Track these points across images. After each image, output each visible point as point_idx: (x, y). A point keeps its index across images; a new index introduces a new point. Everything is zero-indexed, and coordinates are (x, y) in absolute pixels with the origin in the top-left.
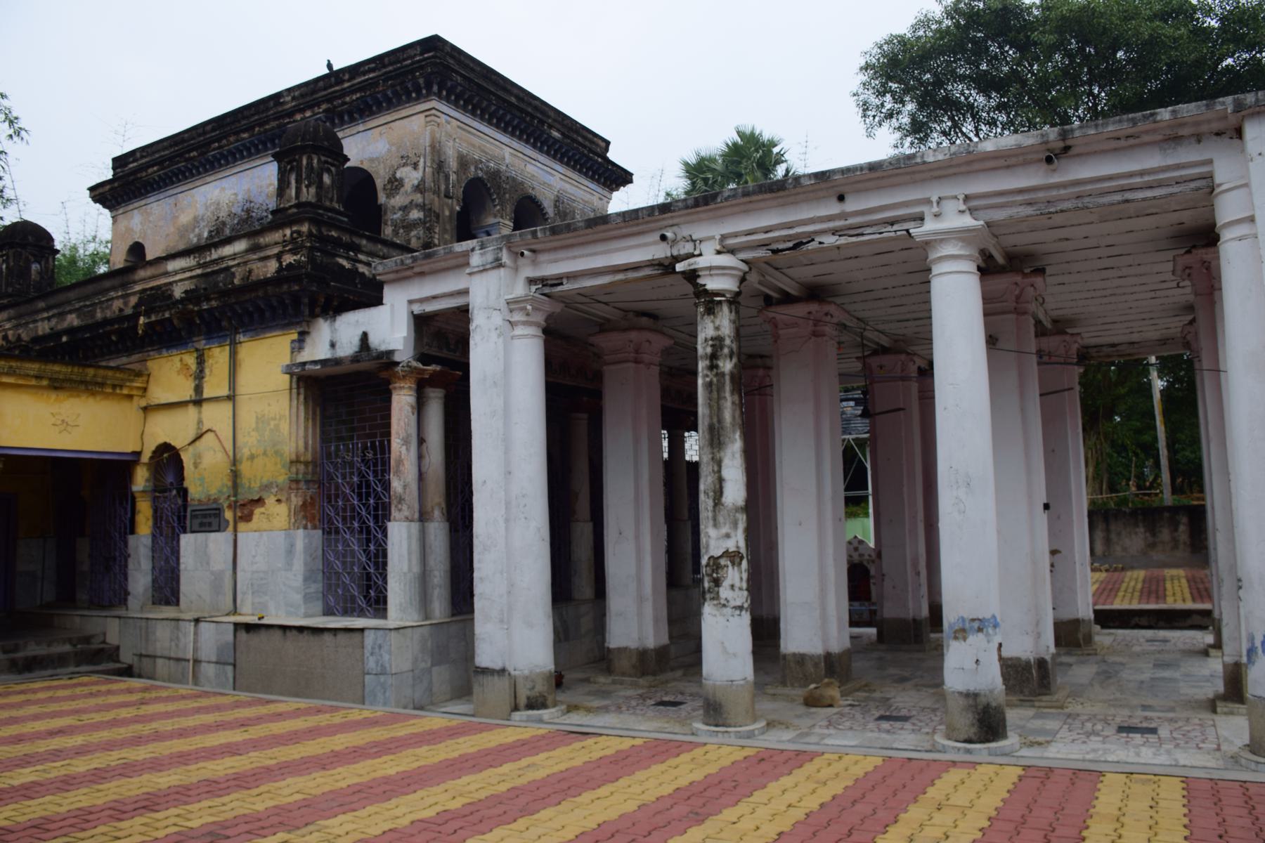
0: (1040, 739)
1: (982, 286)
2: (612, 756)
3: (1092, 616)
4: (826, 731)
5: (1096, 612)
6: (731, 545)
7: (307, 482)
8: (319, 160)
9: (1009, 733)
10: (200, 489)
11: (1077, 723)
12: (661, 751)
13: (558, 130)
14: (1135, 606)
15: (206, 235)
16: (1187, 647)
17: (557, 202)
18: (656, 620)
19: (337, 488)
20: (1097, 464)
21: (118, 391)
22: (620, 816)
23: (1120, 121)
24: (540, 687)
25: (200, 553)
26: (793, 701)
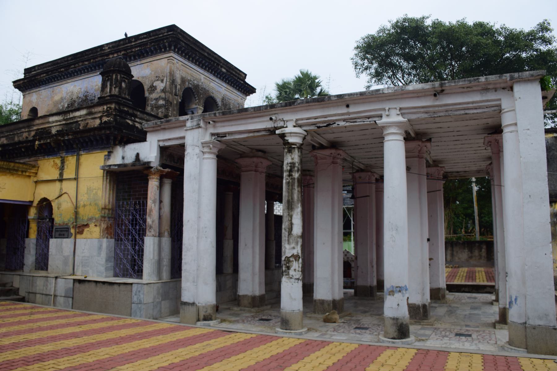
0: (423, 338)
1: (405, 146)
2: (243, 341)
3: (445, 287)
4: (333, 333)
5: (447, 285)
6: (295, 252)
7: (109, 218)
8: (121, 76)
9: (411, 336)
10: (60, 219)
11: (439, 332)
12: (263, 340)
13: (225, 69)
14: (463, 283)
15: (66, 106)
16: (484, 301)
17: (223, 99)
18: (260, 284)
19: (122, 220)
20: (449, 222)
21: (24, 174)
22: (248, 367)
23: (465, 81)
24: (210, 311)
25: (58, 248)
26: (318, 320)
